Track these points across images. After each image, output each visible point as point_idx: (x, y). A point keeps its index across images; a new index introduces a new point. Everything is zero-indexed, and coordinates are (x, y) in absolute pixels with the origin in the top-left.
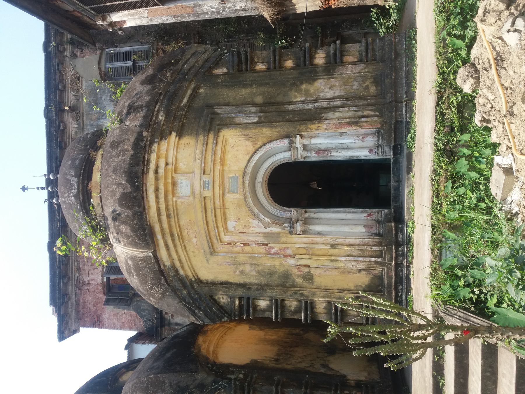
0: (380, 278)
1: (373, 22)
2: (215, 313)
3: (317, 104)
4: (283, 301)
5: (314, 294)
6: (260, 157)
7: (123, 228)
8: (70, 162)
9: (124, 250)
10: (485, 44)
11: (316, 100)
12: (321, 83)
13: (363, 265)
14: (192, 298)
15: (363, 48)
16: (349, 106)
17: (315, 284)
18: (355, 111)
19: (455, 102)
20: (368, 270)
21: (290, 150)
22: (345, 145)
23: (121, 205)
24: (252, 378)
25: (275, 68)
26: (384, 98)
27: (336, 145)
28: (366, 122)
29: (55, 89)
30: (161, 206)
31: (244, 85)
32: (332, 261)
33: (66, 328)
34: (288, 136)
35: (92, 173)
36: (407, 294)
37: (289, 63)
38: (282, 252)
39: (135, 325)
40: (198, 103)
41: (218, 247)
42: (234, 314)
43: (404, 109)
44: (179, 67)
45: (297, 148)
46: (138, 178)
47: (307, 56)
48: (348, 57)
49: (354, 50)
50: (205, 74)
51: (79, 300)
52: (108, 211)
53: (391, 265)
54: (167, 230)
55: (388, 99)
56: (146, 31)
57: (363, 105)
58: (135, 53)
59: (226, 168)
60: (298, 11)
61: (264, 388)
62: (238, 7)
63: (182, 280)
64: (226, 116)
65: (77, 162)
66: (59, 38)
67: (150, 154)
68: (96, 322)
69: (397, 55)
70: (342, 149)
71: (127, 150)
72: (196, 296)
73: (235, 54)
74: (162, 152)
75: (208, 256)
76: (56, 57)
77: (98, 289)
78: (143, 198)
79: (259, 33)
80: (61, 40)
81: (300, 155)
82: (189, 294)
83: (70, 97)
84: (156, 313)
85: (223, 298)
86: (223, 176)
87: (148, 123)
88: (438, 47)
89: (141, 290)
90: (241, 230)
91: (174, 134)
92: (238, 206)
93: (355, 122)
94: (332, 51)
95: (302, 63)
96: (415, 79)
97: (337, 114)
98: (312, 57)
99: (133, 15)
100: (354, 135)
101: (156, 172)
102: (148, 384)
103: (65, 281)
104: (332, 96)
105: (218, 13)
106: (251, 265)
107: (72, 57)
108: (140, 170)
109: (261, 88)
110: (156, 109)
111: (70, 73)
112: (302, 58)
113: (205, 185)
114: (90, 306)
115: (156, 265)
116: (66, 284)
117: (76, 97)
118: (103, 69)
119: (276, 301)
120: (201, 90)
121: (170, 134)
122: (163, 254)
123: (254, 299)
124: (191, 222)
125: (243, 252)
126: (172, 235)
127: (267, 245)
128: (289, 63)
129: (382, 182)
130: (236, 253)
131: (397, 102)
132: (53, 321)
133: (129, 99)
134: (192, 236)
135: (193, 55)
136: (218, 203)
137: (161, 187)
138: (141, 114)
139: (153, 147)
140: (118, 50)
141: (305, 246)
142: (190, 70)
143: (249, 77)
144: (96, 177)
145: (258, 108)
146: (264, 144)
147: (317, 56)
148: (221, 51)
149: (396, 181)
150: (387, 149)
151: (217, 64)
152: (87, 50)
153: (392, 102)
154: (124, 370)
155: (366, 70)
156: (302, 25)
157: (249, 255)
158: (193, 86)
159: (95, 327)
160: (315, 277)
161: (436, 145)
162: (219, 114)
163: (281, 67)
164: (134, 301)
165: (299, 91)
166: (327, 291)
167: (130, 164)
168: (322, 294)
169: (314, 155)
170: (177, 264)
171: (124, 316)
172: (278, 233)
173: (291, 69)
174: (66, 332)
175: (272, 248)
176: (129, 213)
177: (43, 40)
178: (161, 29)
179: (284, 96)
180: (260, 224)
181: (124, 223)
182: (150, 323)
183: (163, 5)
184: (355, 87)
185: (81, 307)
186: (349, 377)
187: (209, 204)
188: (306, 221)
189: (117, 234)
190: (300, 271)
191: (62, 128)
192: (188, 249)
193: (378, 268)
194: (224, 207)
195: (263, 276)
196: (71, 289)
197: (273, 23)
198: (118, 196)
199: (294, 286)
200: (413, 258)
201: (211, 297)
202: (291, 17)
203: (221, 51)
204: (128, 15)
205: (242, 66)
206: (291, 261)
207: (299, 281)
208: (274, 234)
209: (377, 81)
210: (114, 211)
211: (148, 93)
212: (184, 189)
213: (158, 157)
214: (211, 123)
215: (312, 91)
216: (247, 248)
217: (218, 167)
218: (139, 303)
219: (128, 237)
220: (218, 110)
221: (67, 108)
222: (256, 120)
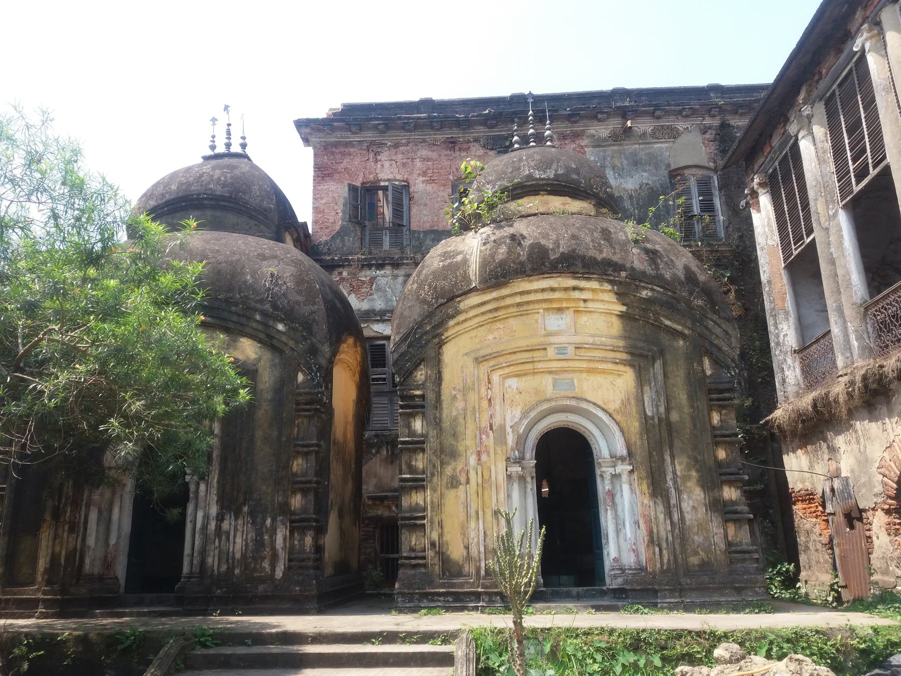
0: (460, 574)
1: (774, 567)
2: (405, 365)
3: (673, 490)
4: (423, 450)
5: (434, 490)
6: (600, 419)
7: (503, 250)
8: (574, 166)
9: (475, 250)
10: (766, 667)
11: (677, 490)
12: (699, 495)
13: (474, 551)
14: (421, 337)
15: (745, 547)
16: (672, 531)
17: (447, 492)
18: (667, 539)
19: (695, 650)
20: (468, 558)
21: (611, 457)
22: (621, 527)
23: (532, 246)
24: (322, 413)
25: (716, 436)
26: (685, 575)
27: (621, 517)
28: (654, 553)
29: (656, 105)
30: (532, 295)
31: (691, 398)
32: (477, 512)
33: (313, 129)
34: (630, 454)
35: (561, 196)
36: (443, 607)
37: (722, 454)
38: (483, 449)
39: (321, 228)
40: (665, 339)
41: (485, 367)
42: (404, 390)
43: (673, 600)
44: (710, 315)
45: (614, 466)
46: (567, 267)
47: (733, 477)
48: (733, 529)
49: (742, 536)
50: (703, 347)
51: (353, 146)
52: (520, 227)
53: (478, 587)
54: (502, 303)
55: (683, 580)
56: (745, 233)
57: (674, 549)
58: (713, 218)
59: (584, 375)
60: (785, 457)
61: (314, 429)
62: (787, 373)
63: (442, 324)
64: (652, 375)
65: (575, 176)
66: (729, 108)
67: (597, 280)
68: (322, 173)
69: (739, 590)
70: (617, 525)
71: (601, 252)
73: (730, 386)
74: (601, 294)
75: (473, 355)
76: (702, 105)
77: (370, 174)
78: (543, 274)
79: (750, 399)
80: (726, 110)
81: (604, 472)
82: (426, 333)
83: (644, 126)
84: (340, 259)
86: (574, 371)
87: (637, 278)
88: (756, 631)
89: (424, 272)
90: (506, 396)
91: (624, 309)
92: (537, 392)
93: (653, 540)
94: (739, 508)
95: (724, 470)
96: (711, 612)
97: (661, 517)
98: (730, 483)
99: (769, 225)
100: (636, 539)
101: (575, 288)
102: (308, 282)
103: (380, 127)
104: (684, 510)
105: (778, 344)
106: (465, 410)
107: (702, 127)
108: (577, 270)
109: (688, 418)
110: (655, 287)
111: (681, 125)
112: (728, 470)
113: (561, 350)
114: (345, 163)
115: (460, 292)
116: (375, 127)
117: (644, 134)
118: (687, 172)
119: (423, 442)
120: (681, 342)
121: (623, 304)
122: (474, 299)
123: (423, 413)
124: (513, 332)
125: (480, 399)
126: (496, 310)
127: (491, 429)
128: (722, 454)
129: (564, 578)
130: (479, 390)
131: (681, 590)
132: (321, 112)
133: (665, 250)
134: (496, 334)
135: (726, 333)
136: (539, 365)
137: (557, 295)
138: (650, 270)
139: (606, 284)
140: (716, 193)
141: (493, 478)
142: (707, 328)
143: (703, 404)
144: (556, 203)
145: (664, 416)
146: (618, 424)
147: (733, 489)
148: (733, 368)
149: (578, 593)
150: (620, 580)
151: (715, 362)
152: (713, 148)
153: (680, 584)
155: (718, 552)
156: (765, 462)
157: (477, 407)
158: (686, 332)
160: (455, 490)
161: (644, 631)
162: (653, 365)
163: (717, 444)
164: (354, 227)
165: (689, 468)
166: (438, 507)
167: (584, 257)
168: (435, 500)
169: (607, 488)
170: (461, 318)
171: (333, 213)
172: (506, 444)
173: (716, 457)
174: (307, 130)
175: (488, 436)
176: (523, 258)
177: (723, 84)
178: (749, 256)
179: (681, 449)
180: (516, 420)
181: (510, 252)
182: (325, 250)
183: (785, 267)
184: (696, 538)
185: (342, 149)
186: (327, 536)
187: (537, 355)
188: (522, 479)
189: (495, 241)
190: (460, 471)
191: (599, 116)
192: (479, 329)
193: (473, 571)
194: (535, 373)
195: (451, 424)
196: (369, 136)
197: (767, 422)
198: (543, 242)
199: (442, 464)
200: (489, 614)
201: (423, 360)
202: (775, 445)
203: (733, 368)
204: (769, 219)
205: (713, 393)
206: (473, 460)
207: (449, 471)
208: (505, 437)
209: (705, 566)
210: (524, 237)
211: (675, 277)
212: (554, 322)
213: (593, 290)
214: (641, 355)
215: (689, 484)
216: (485, 403)
217: (585, 366)
218: (352, 234)
219: (492, 256)
220: (658, 365)
221: (629, 123)
222: (649, 413)
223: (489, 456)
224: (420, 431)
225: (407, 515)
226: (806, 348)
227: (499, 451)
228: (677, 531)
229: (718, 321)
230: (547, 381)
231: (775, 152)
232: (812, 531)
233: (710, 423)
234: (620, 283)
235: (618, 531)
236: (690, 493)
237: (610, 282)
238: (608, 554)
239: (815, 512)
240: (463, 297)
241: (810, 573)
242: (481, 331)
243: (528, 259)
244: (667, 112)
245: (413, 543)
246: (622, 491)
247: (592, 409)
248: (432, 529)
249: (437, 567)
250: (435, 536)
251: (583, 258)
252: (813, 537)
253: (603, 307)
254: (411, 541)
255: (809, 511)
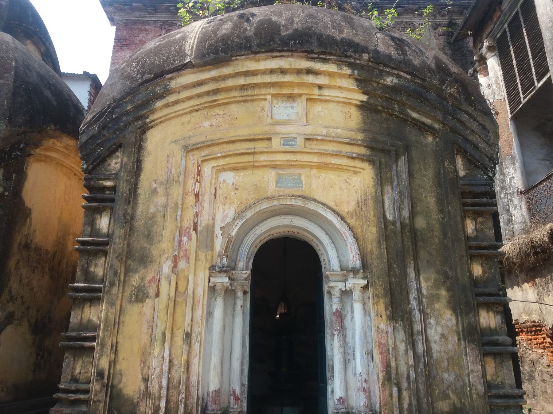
2: (95, 149)
5: (112, 304)
6: (330, 223)
11: (422, 312)
12: (450, 320)
13: (154, 385)
14: (119, 118)
16: (416, 366)
17: (129, 306)
18: (408, 376)
21: (342, 270)
23: (261, 23)
25: (470, 248)
27: (350, 344)
28: (391, 395)
31: (440, 201)
32: (164, 334)
33: (116, 8)
34: (365, 265)
37: (477, 270)
38: (182, 254)
41: (196, 157)
44: (465, 107)
45: (345, 281)
46: (301, 44)
47: (492, 299)
48: (493, 365)
51: (149, 24)
54: (222, 85)
57: (418, 389)
59: (314, 172)
63: (147, 103)
64: (394, 172)
67: (335, 62)
70: (345, 354)
71: (341, 32)
72: (122, 124)
74: (338, 80)
75: (182, 143)
78: (271, 51)
81: (333, 286)
82: (127, 113)
85: (116, 163)
86: (302, 166)
87: (380, 61)
90: (219, 192)
91: (365, 98)
92: (257, 188)
93: (390, 377)
95: (481, 290)
97: (402, 347)
100: (368, 374)
101: (309, 71)
105: (503, 188)
106: (165, 206)
107: (434, 24)
108: (312, 48)
109: (437, 226)
110: (402, 74)
112: (487, 290)
113: (289, 140)
119: (106, 244)
120: (430, 138)
121: (364, 93)
123: (112, 209)
124: (235, 120)
125: (185, 193)
126: (215, 92)
127: (195, 229)
128: (477, 270)
134: (214, 121)
136: (262, 158)
137: (287, 78)
139: (345, 68)
141: (190, 291)
142: (461, 122)
143: (455, 208)
145: (407, 221)
146: (351, 229)
147: (491, 314)
152: (442, 40)
154: (43, 49)
155: (475, 396)
157: (180, 203)
158: (436, 126)
159: (115, 42)
160: (140, 305)
163: (472, 257)
165: (437, 285)
166: (116, 325)
168: (111, 317)
170: (172, 98)
172: (212, 248)
173: (471, 274)
175: (190, 239)
179: (428, 262)
180: (228, 221)
183: (511, 119)
184: (446, 376)
185: (140, 26)
187: (260, 146)
188: (229, 293)
190: (150, 281)
192: (194, 114)
194: (255, 167)
201: (120, 146)
204: (497, 77)
206: (167, 268)
207: (135, 280)
208: (212, 241)
211: (424, 65)
212: (283, 111)
213: (330, 75)
214: (382, 151)
215: (437, 306)
216: (191, 199)
219: (215, 32)
220: (402, 161)
222: (390, 217)
223: (188, 262)
224: (105, 230)
225: (74, 334)
226: (533, 188)
227: (202, 256)
228: (421, 366)
229: (474, 114)
230: (268, 180)
231: (505, 15)
232: (538, 362)
233: (464, 232)
234: (361, 68)
235: (346, 363)
236: (438, 317)
237: (351, 65)
238: (332, 391)
239: (542, 343)
240: (174, 74)
241: (534, 402)
242: (195, 117)
243: (256, 34)
244: (406, 10)
245: (77, 371)
246: (352, 312)
247: (321, 210)
248: (101, 354)
249: (102, 405)
250: (104, 363)
251: (320, 36)
252: (539, 368)
253: (341, 95)
254: (74, 369)
255: (535, 342)
